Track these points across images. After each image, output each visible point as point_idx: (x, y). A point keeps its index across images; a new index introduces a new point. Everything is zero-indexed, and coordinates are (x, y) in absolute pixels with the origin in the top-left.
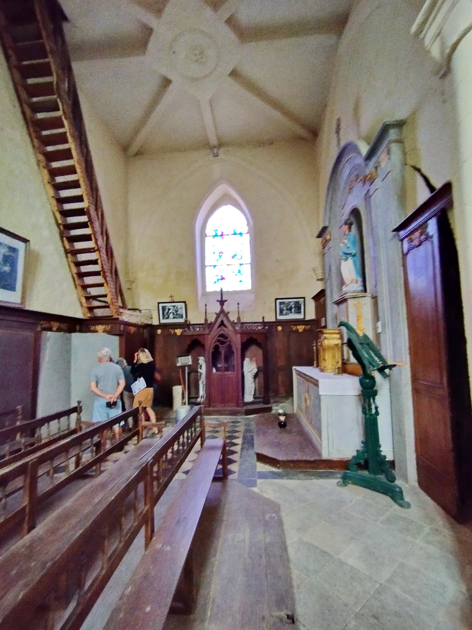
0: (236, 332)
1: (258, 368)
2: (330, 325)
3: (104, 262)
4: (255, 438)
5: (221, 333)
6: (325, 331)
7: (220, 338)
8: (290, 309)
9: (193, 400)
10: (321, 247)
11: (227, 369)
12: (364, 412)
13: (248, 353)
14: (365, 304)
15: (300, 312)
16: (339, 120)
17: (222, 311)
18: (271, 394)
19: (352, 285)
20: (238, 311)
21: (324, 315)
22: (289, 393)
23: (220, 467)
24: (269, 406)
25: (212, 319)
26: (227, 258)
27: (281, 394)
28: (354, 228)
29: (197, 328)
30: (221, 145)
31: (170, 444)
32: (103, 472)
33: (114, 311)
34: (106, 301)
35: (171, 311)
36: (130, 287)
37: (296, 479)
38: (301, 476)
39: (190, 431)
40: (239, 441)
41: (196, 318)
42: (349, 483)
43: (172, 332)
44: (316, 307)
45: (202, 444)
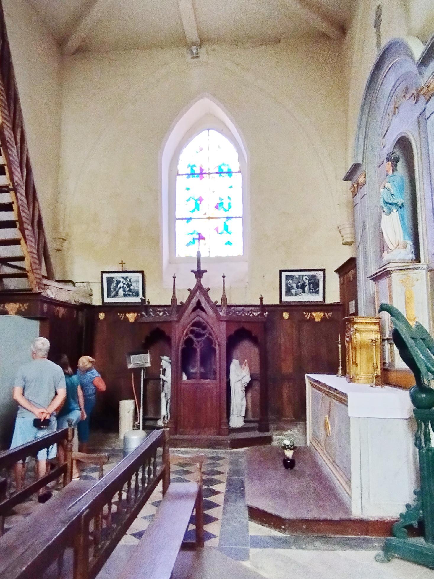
0: (219, 319)
1: (251, 376)
2: (362, 312)
3: (21, 208)
4: (246, 484)
5: (197, 319)
6: (356, 319)
7: (195, 328)
8: (303, 287)
9: (150, 423)
10: (351, 195)
11: (204, 376)
12: (417, 444)
13: (237, 352)
14: (417, 280)
15: (317, 292)
16: (379, 7)
17: (199, 287)
18: (272, 417)
19: (397, 251)
20: (224, 287)
21: (355, 297)
22: (300, 415)
23: (193, 527)
24: (267, 434)
25: (182, 297)
26: (208, 207)
27: (286, 417)
28: (401, 166)
29: (160, 312)
30: (202, 41)
31: (116, 486)
32: (8, 530)
33: (35, 282)
34: (24, 267)
35: (121, 285)
36: (59, 247)
37: (310, 549)
38: (318, 544)
39: (147, 469)
40: (221, 488)
41: (158, 296)
42: (393, 557)
43: (122, 316)
44: (342, 285)
45: (164, 492)
